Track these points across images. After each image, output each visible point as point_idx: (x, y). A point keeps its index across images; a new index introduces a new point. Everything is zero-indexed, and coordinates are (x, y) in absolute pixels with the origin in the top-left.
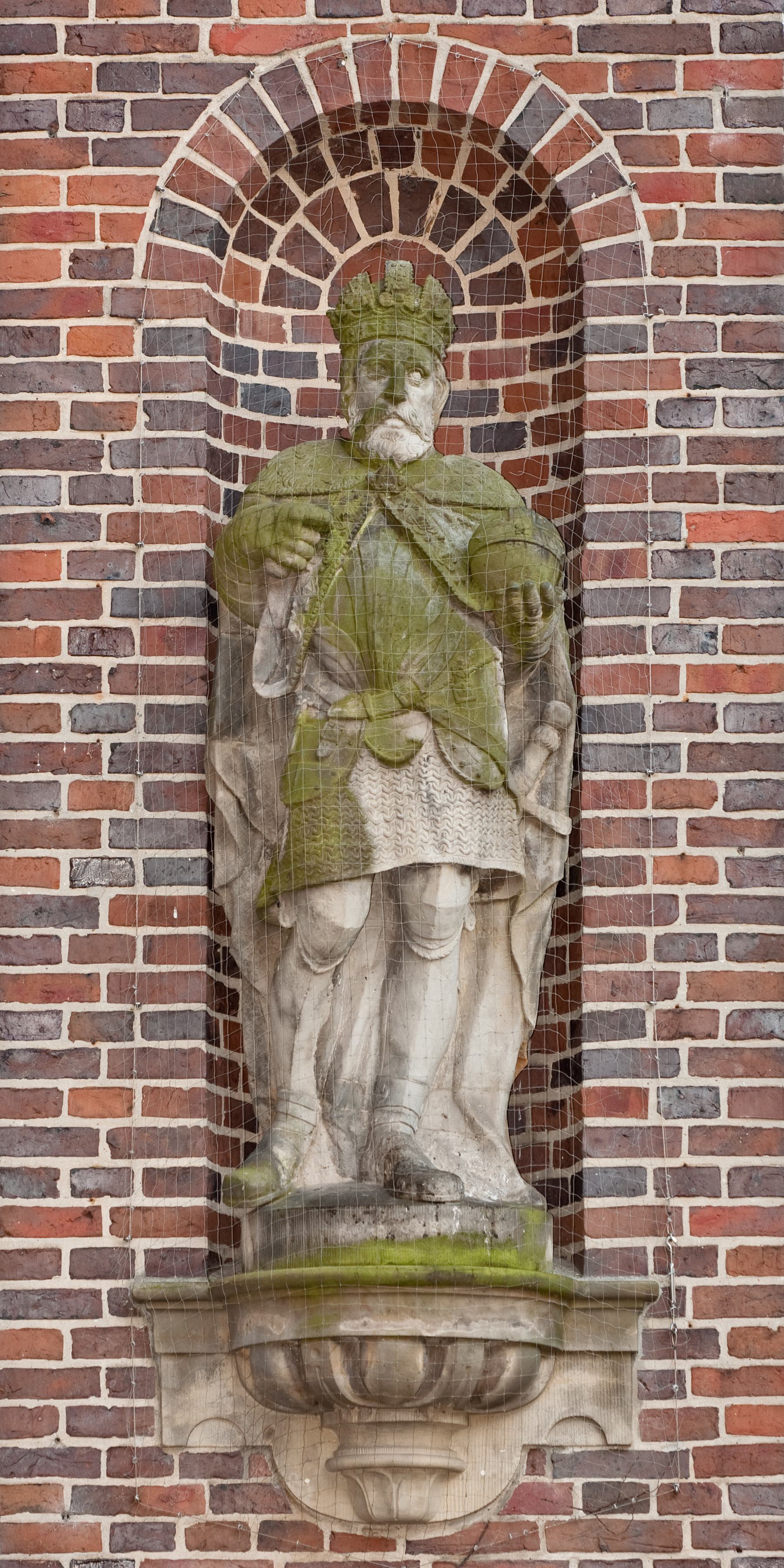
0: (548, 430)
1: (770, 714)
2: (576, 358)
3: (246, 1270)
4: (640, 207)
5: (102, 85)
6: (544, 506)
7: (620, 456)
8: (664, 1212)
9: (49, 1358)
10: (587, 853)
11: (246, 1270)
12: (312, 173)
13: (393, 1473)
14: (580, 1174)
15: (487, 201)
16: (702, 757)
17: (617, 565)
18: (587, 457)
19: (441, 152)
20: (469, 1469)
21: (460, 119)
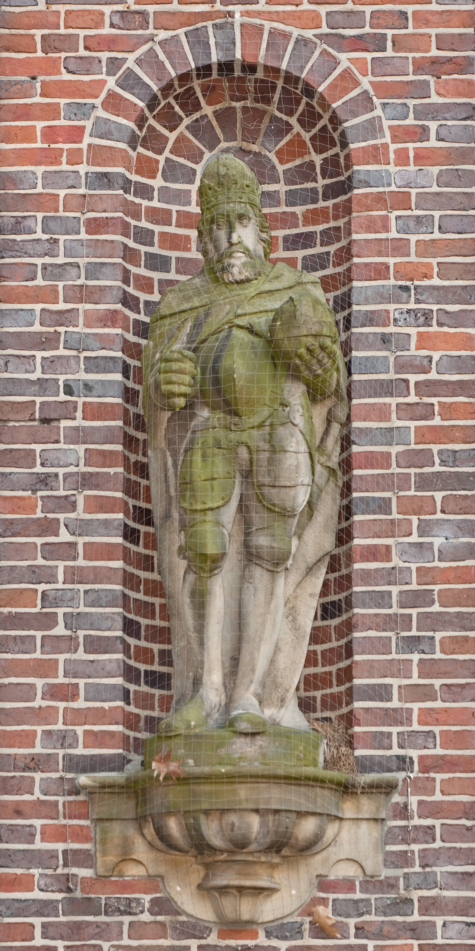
0: (329, 236)
1: (470, 409)
2: (348, 704)
3: (158, 795)
4: (386, 124)
5: (77, 139)
6: (327, 284)
7: (372, 667)
8: (401, 759)
9: (52, 818)
10: (355, 449)
11: (158, 795)
12: (190, 103)
13: (240, 892)
14: (351, 595)
15: (293, 121)
16: (425, 482)
17: (373, 553)
18: (354, 275)
19: (264, 91)
20: (283, 890)
21: (277, 70)
